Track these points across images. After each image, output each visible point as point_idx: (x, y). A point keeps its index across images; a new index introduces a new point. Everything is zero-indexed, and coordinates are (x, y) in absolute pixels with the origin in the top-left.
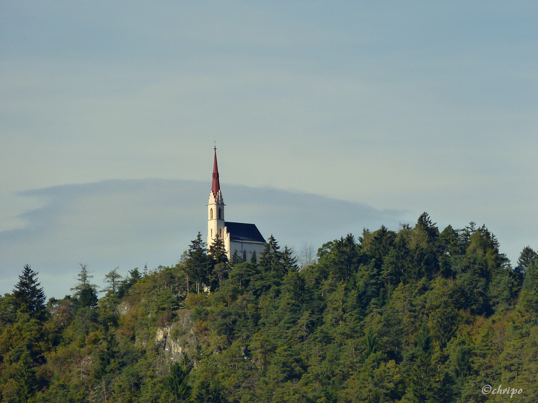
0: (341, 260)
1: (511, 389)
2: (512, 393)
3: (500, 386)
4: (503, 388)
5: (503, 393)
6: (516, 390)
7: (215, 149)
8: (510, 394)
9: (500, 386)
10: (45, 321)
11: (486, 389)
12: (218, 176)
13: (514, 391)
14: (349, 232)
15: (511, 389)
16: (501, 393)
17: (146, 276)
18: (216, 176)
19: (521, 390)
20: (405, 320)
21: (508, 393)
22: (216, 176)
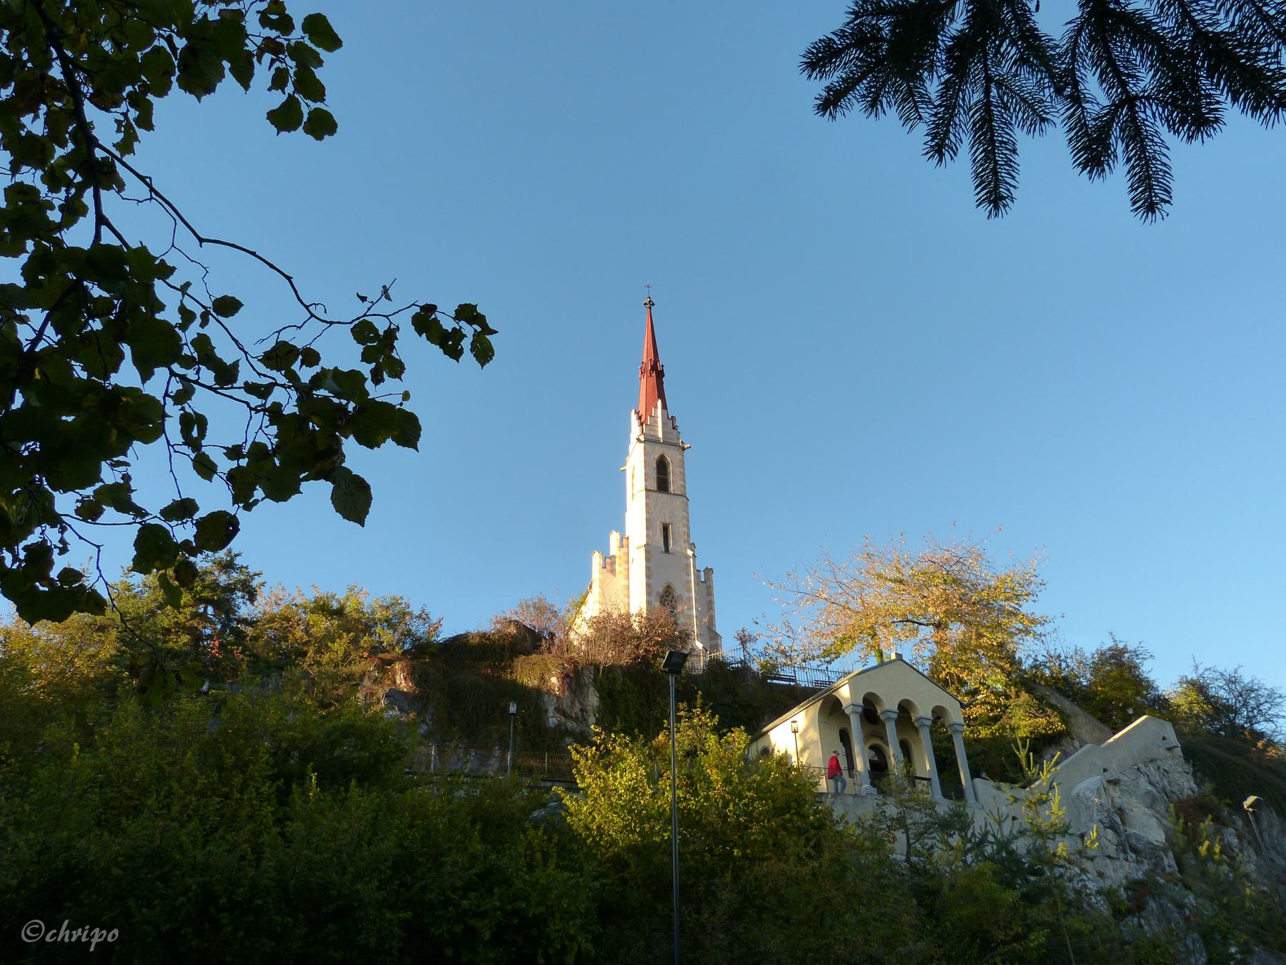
0: (977, 711)
1: (90, 930)
2: (95, 940)
3: (66, 922)
4: (71, 928)
5: (73, 940)
6: (104, 932)
7: (651, 304)
8: (89, 943)
9: (66, 922)
10: (635, 846)
11: (33, 931)
12: (660, 375)
13: (97, 936)
14: (531, 594)
15: (90, 930)
16: (66, 940)
17: (588, 641)
18: (236, 341)
19: (116, 931)
20: (124, 820)
21: (84, 939)
22: (236, 341)
